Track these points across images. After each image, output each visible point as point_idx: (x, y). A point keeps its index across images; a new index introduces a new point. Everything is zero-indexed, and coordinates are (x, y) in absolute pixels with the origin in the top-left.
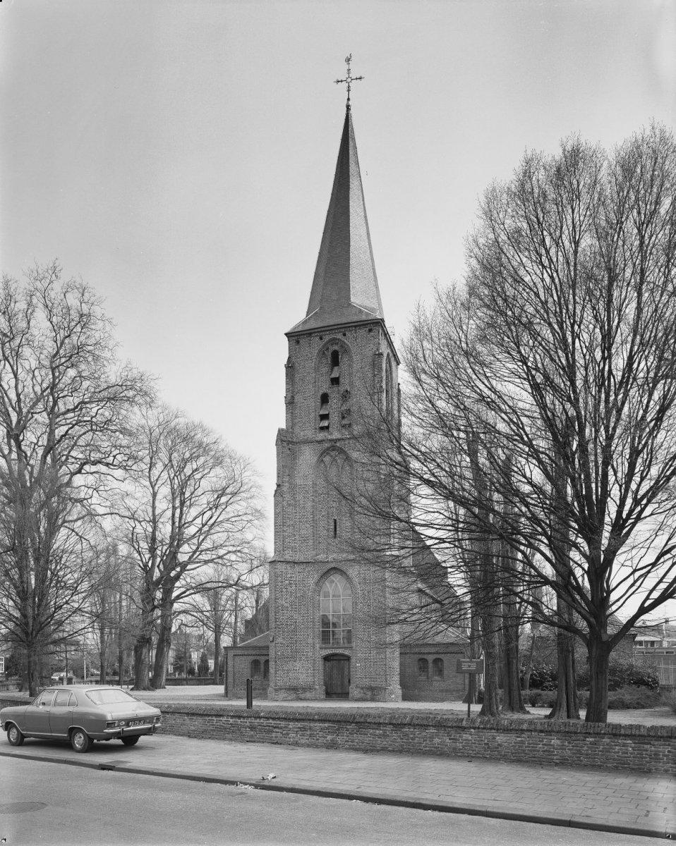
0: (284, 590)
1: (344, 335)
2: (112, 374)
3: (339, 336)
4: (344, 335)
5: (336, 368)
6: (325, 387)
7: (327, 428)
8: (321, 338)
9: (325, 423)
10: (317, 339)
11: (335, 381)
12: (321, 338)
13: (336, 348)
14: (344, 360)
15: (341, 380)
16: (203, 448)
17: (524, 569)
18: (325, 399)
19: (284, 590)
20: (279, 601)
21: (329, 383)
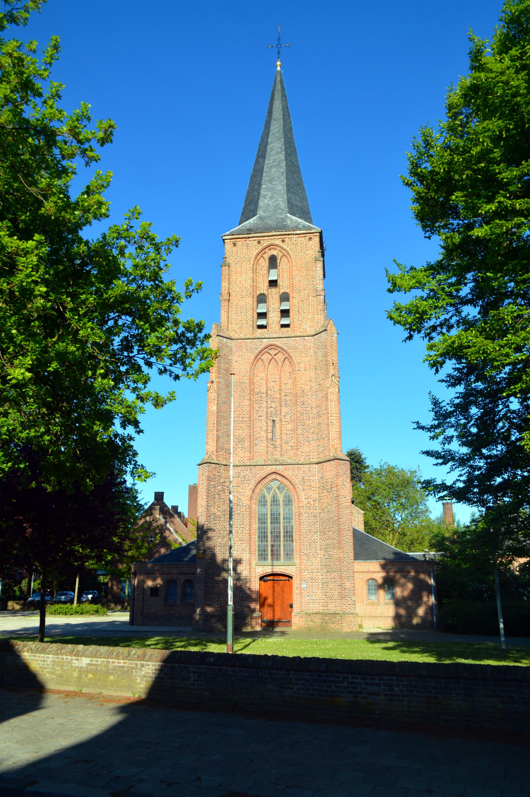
0: (217, 496)
1: (283, 241)
2: (367, 464)
3: (278, 242)
4: (283, 241)
5: (272, 271)
6: (263, 288)
7: (288, 326)
8: (259, 242)
9: (285, 321)
10: (255, 243)
11: (273, 283)
12: (259, 242)
13: (275, 252)
14: (283, 263)
15: (280, 282)
16: (450, 442)
17: (102, 368)
18: (262, 299)
19: (217, 496)
20: (212, 509)
21: (267, 284)
